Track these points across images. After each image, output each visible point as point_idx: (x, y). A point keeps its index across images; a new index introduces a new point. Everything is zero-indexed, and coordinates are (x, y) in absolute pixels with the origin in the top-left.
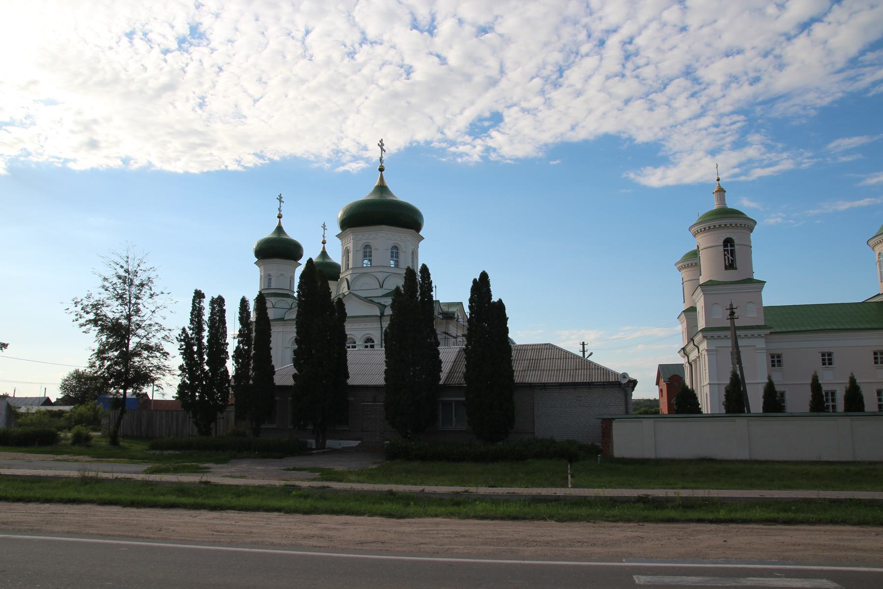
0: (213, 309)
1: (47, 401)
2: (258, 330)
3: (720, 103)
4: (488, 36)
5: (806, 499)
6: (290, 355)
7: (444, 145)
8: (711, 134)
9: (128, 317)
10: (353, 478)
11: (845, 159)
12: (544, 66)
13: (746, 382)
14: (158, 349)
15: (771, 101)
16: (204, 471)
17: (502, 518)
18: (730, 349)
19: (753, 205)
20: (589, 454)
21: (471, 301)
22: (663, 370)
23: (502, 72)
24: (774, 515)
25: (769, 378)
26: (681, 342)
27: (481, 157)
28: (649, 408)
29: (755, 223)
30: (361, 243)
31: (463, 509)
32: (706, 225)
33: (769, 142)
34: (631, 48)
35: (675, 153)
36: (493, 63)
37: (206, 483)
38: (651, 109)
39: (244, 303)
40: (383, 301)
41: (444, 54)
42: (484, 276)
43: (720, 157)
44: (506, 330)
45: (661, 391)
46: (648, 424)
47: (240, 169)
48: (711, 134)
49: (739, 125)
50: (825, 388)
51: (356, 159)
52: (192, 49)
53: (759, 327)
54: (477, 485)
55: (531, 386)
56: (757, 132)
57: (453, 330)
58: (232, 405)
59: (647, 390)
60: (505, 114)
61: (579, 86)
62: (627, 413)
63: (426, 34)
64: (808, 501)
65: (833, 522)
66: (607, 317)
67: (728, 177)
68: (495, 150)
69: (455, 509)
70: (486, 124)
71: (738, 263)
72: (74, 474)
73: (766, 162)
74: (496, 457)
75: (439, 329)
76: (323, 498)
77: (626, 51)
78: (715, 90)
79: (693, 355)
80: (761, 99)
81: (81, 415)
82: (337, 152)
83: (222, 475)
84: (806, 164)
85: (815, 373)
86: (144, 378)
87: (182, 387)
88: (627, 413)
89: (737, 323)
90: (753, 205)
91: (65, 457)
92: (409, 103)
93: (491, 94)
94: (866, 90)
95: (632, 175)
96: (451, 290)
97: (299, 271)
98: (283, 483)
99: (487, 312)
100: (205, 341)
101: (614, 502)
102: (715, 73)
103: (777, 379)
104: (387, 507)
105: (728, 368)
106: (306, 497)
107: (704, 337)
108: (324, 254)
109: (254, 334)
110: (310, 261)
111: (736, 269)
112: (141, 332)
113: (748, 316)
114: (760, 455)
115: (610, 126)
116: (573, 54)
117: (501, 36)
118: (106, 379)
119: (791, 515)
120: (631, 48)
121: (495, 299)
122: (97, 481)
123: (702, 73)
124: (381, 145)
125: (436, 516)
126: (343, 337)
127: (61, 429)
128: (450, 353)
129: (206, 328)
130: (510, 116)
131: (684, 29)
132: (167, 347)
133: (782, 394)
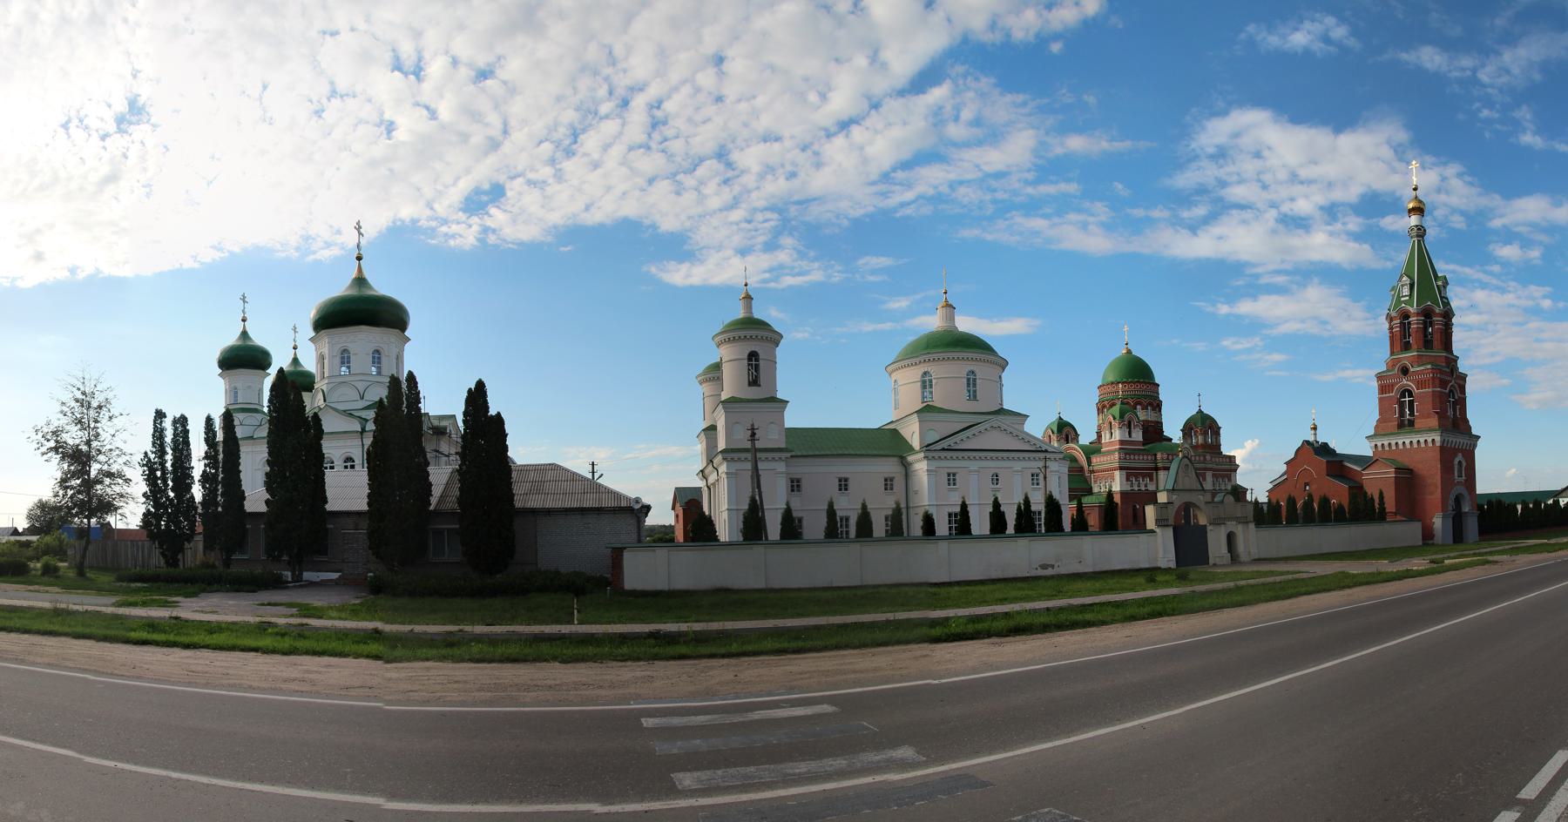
0: (176, 429)
1: (15, 532)
2: (225, 451)
3: (754, 195)
4: (489, 82)
6: (260, 478)
7: (434, 224)
8: (741, 230)
9: (88, 443)
10: (334, 614)
11: (872, 278)
12: (554, 127)
14: (120, 475)
15: (804, 202)
16: (174, 605)
17: (501, 661)
19: (781, 316)
20: (598, 587)
21: (465, 414)
22: (679, 492)
23: (505, 132)
24: (785, 645)
26: (700, 463)
27: (478, 240)
28: (663, 536)
30: (338, 347)
31: (456, 651)
32: (730, 335)
34: (659, 114)
36: (494, 119)
37: (176, 618)
38: (678, 193)
39: (209, 421)
40: (364, 414)
41: (433, 106)
42: (480, 385)
43: (750, 259)
44: (506, 448)
46: (661, 554)
47: (196, 265)
48: (741, 230)
49: (772, 223)
50: (839, 514)
51: (328, 245)
52: (132, 128)
54: (473, 624)
55: (534, 512)
56: (791, 234)
57: (444, 448)
58: (1110, 453)
59: (662, 515)
60: (508, 186)
61: (596, 156)
62: (639, 541)
63: (412, 77)
65: (838, 647)
66: (617, 435)
68: (494, 231)
69: (449, 651)
70: (485, 198)
71: (762, 380)
72: (47, 605)
74: (495, 592)
75: (429, 447)
76: (301, 636)
77: (653, 117)
78: (749, 180)
79: (712, 479)
80: (796, 198)
81: (47, 545)
82: (307, 238)
83: (193, 609)
84: (837, 278)
86: (107, 507)
87: (147, 515)
88: (639, 541)
89: (758, 445)
90: (781, 316)
91: (36, 587)
92: (391, 170)
93: (492, 160)
94: (895, 210)
95: (653, 270)
96: (442, 401)
97: (268, 382)
98: (258, 619)
99: (483, 427)
100: (169, 465)
101: (623, 638)
102: (750, 158)
103: (795, 505)
104: (374, 647)
106: (283, 635)
108: (295, 361)
109: (221, 457)
110: (281, 371)
112: (101, 458)
114: (776, 584)
115: (630, 209)
116: (589, 114)
117: (505, 83)
118: (70, 509)
119: (800, 644)
120: (659, 114)
121: (492, 412)
122: (68, 613)
123: (735, 156)
124: (358, 228)
125: (427, 659)
126: (319, 457)
127: (31, 559)
128: (441, 475)
129: (169, 450)
130: (514, 188)
131: (719, 99)
132: (128, 473)
133: (800, 520)
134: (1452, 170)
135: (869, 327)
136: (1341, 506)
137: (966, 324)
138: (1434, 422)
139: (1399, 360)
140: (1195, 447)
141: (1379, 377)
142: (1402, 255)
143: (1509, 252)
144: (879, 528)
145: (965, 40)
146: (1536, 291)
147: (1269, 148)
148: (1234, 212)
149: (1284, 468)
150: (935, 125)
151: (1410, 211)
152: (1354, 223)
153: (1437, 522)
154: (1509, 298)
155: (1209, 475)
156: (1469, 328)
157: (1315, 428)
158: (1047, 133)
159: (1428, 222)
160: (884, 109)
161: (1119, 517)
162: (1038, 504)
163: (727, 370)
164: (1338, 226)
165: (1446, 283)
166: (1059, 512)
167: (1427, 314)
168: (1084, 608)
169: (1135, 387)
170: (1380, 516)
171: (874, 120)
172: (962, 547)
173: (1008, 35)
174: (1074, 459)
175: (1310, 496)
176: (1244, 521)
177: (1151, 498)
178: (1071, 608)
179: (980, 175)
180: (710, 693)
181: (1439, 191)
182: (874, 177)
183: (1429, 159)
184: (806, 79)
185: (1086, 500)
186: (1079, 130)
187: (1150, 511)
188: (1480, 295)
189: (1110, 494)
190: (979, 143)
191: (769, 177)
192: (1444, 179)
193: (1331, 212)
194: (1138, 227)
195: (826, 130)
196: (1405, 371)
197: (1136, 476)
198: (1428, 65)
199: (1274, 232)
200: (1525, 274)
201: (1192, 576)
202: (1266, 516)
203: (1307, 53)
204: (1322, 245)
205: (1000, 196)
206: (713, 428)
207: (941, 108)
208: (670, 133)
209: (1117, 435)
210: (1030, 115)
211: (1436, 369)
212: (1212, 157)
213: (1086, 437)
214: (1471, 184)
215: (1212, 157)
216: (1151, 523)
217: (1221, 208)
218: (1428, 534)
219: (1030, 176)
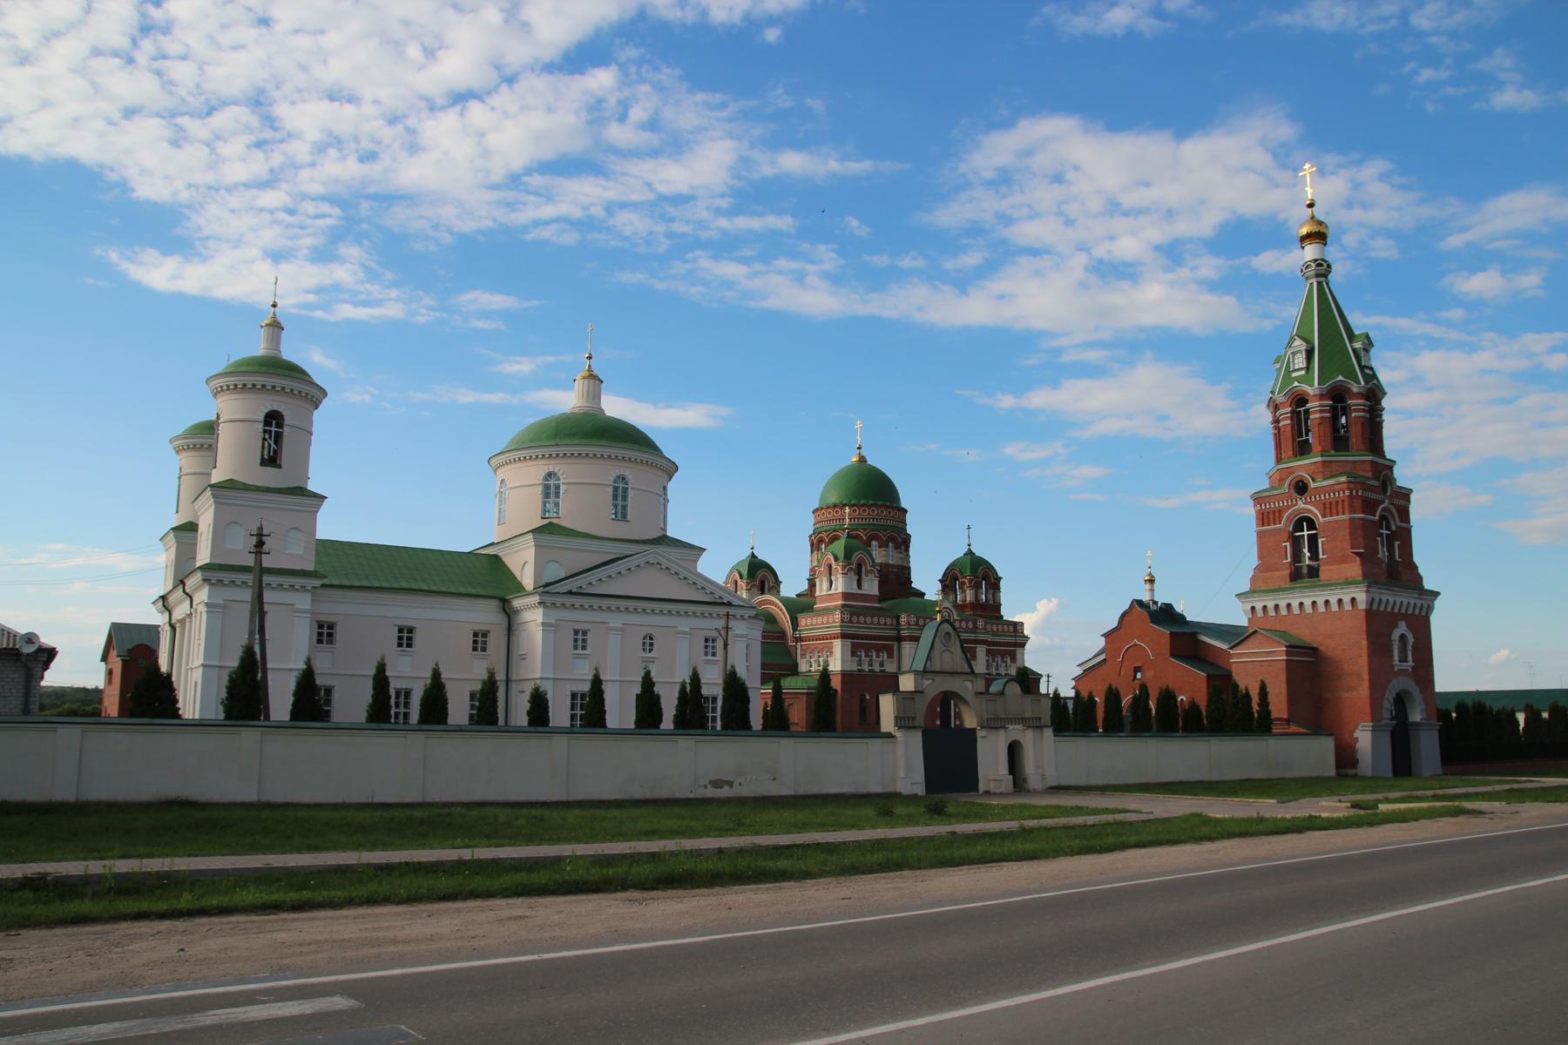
3: (305, 174)
11: (480, 324)
15: (389, 199)
19: (329, 363)
22: (118, 631)
24: (278, 896)
25: (308, 662)
26: (161, 585)
28: (81, 705)
29: (325, 394)
32: (239, 380)
33: (373, 265)
35: (208, 238)
43: (287, 268)
45: (110, 673)
46: (69, 736)
49: (329, 221)
50: (394, 685)
59: (79, 667)
61: (27, 42)
67: (294, 306)
77: (144, 16)
79: (180, 611)
80: (372, 190)
84: (424, 317)
89: (267, 562)
90: (329, 363)
94: (525, 229)
95: (114, 256)
102: (307, 119)
107: (204, 580)
113: (287, 552)
114: (277, 796)
115: (84, 147)
123: (282, 110)
131: (264, 22)
133: (329, 691)
134: (1371, 171)
135: (467, 397)
136: (1194, 707)
137: (615, 407)
138: (1354, 569)
139: (1290, 471)
140: (960, 608)
141: (1258, 499)
142: (1292, 310)
143: (1483, 284)
144: (459, 709)
145: (642, 15)
146: (1536, 342)
147: (1076, 168)
148: (1023, 260)
149: (1101, 642)
150: (590, 123)
151: (1303, 239)
152: (1210, 267)
153: (1364, 738)
154: (1484, 359)
155: (981, 651)
156: (1409, 414)
157: (1151, 581)
158: (752, 146)
159: (1332, 253)
160: (520, 87)
161: (838, 711)
162: (713, 685)
163: (225, 435)
164: (1184, 272)
165: (1368, 343)
166: (746, 700)
167: (1337, 397)
168: (778, 851)
169: (869, 514)
170: (1261, 725)
171: (504, 98)
172: (589, 747)
173: (704, 13)
174: (771, 619)
175: (1143, 688)
176: (1036, 725)
177: (890, 683)
178: (757, 851)
179: (652, 196)
180: (128, 982)
181: (1349, 204)
182: (497, 178)
183: (1330, 159)
184: (407, 24)
185: (788, 684)
186: (798, 145)
187: (887, 703)
188: (1429, 361)
189: (825, 675)
190: (654, 153)
191: (333, 152)
192: (1356, 186)
193: (1173, 253)
194: (878, 281)
195: (426, 99)
196: (1301, 488)
197: (867, 649)
198: (1324, 25)
199: (1083, 286)
200: (1510, 318)
201: (950, 809)
202: (1071, 718)
203: (1132, 34)
204: (1159, 301)
205: (678, 227)
206: (189, 528)
207: (600, 101)
208: (173, 48)
209: (840, 585)
210: (729, 120)
211: (1356, 482)
212: (990, 184)
213: (793, 585)
214: (1402, 187)
215: (990, 184)
216: (887, 722)
217: (1003, 255)
218: (1346, 758)
219: (724, 204)
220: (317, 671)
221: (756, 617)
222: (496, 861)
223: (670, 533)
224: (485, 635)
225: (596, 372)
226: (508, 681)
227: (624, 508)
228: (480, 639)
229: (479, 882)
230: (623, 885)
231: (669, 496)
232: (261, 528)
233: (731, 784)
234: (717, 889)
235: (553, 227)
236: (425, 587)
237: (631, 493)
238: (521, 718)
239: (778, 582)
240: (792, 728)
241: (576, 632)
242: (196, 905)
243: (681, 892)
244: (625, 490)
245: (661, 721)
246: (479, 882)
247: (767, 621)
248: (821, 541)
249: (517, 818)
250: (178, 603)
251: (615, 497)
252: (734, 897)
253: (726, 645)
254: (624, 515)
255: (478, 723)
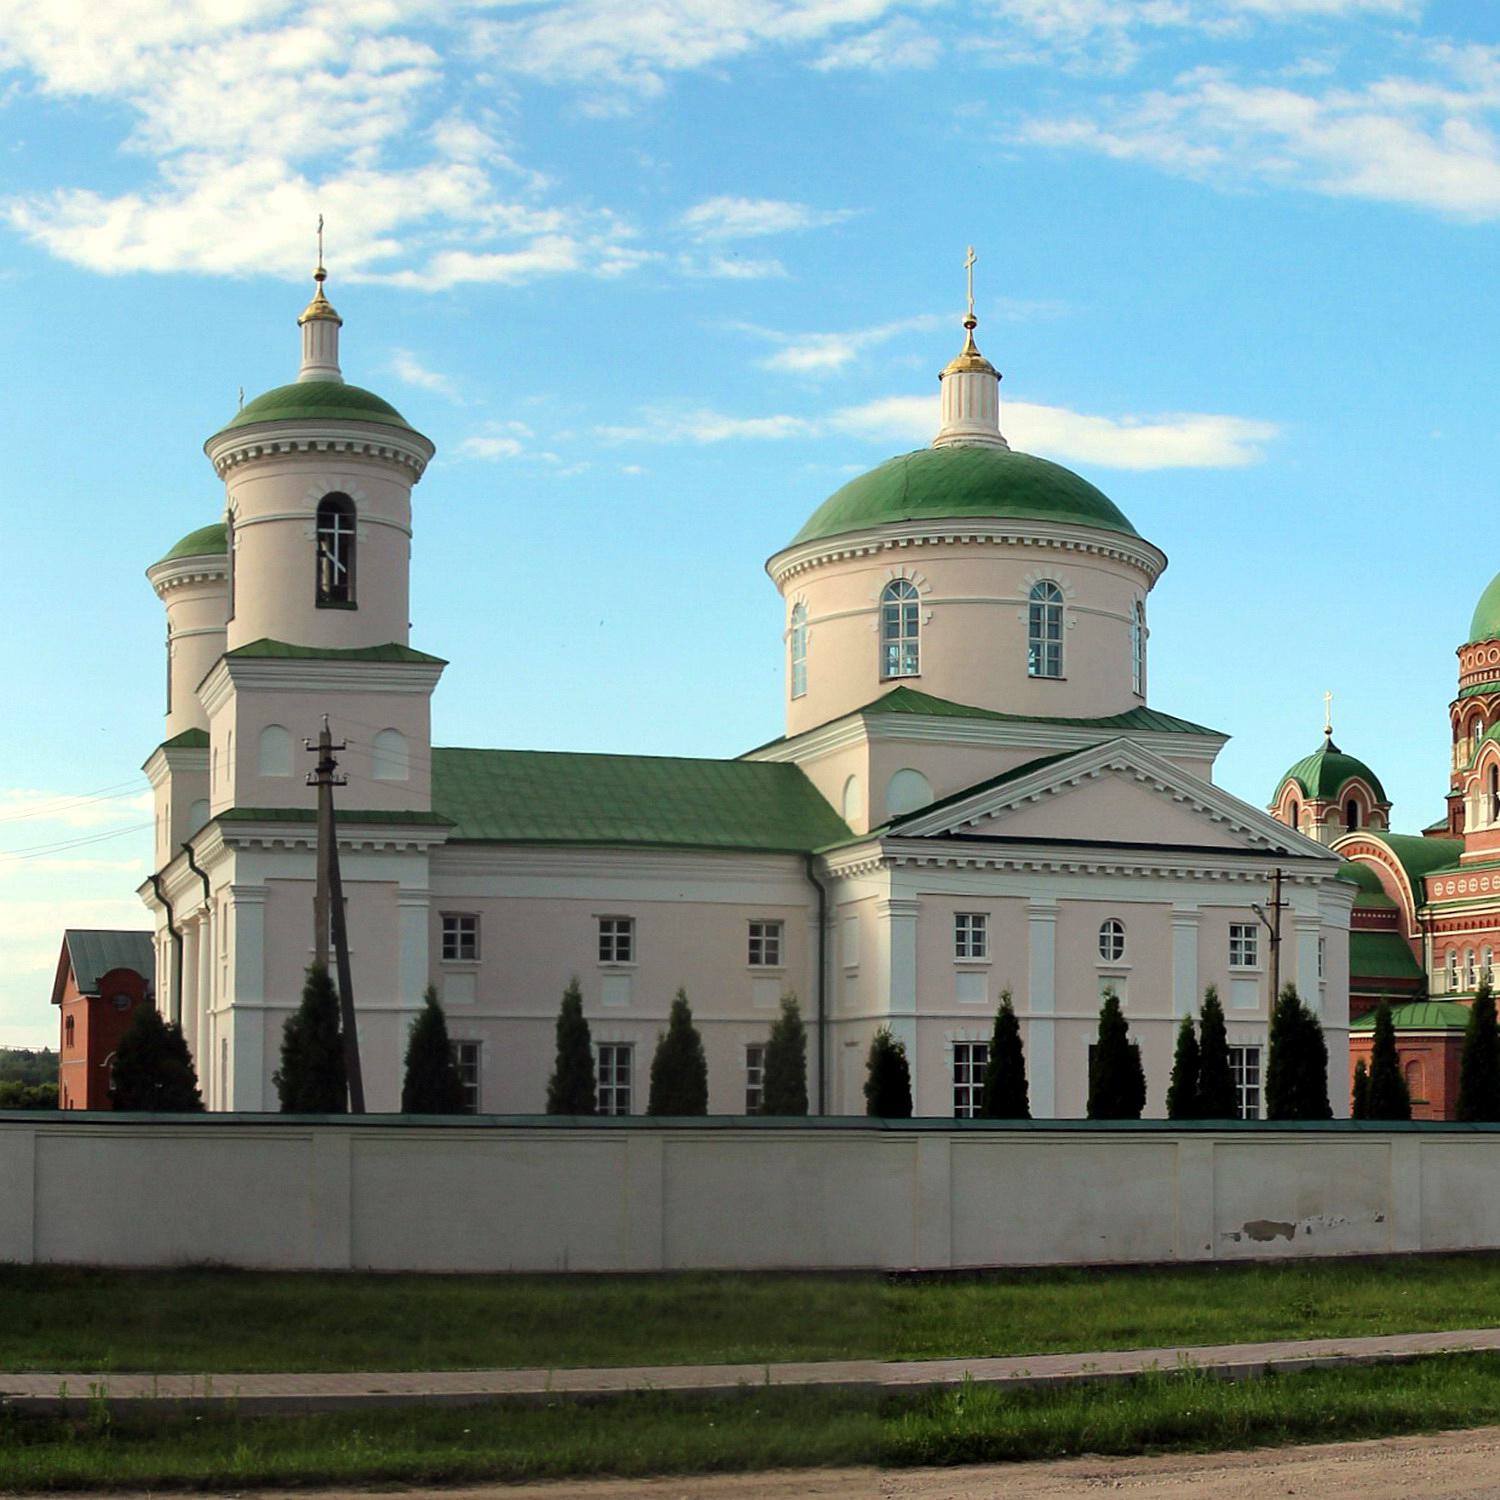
5: (511, 1397)
11: (732, 270)
13: (357, 1005)
18: (312, 891)
19: (429, 380)
22: (79, 946)
24: (406, 1457)
25: (431, 996)
26: (151, 855)
29: (430, 449)
33: (508, 163)
35: (185, 150)
43: (337, 191)
45: (69, 1024)
48: (315, 96)
49: (412, 78)
50: (598, 1035)
53: (410, 819)
56: (472, 116)
64: (515, 1405)
67: (356, 269)
73: (487, 235)
79: (188, 904)
84: (617, 264)
85: (575, 985)
89: (343, 800)
90: (429, 380)
94: (815, 47)
95: (20, 216)
103: (457, 999)
105: (301, 951)
107: (229, 842)
111: (353, 607)
113: (381, 779)
114: (385, 1256)
119: (457, 1454)
133: (471, 1050)
135: (715, 429)
137: (1031, 430)
144: (728, 1085)
162: (1249, 1025)
163: (248, 553)
166: (1320, 1056)
168: (1388, 1369)
174: (1370, 884)
178: (1344, 1370)
185: (1406, 1018)
206: (194, 741)
213: (1414, 810)
220: (448, 1012)
221: (1337, 880)
222: (812, 1390)
223: (1157, 701)
224: (774, 928)
225: (984, 357)
226: (822, 1022)
227: (1055, 651)
228: (764, 938)
229: (784, 1435)
230: (1071, 1445)
231: (1150, 624)
232: (326, 735)
233: (1289, 1230)
234: (1264, 1453)
235: (874, 38)
236: (649, 836)
237: (1067, 619)
238: (851, 1094)
239: (1384, 804)
240: (1417, 1113)
241: (961, 919)
242: (260, 1467)
243: (1188, 1459)
244: (1056, 613)
245: (1141, 1102)
246: (784, 1435)
247: (1362, 889)
248: (1475, 715)
249: (853, 1303)
250: (184, 888)
251: (1035, 628)
252: (1300, 1468)
253: (1275, 940)
254: (1055, 666)
255: (769, 1110)
